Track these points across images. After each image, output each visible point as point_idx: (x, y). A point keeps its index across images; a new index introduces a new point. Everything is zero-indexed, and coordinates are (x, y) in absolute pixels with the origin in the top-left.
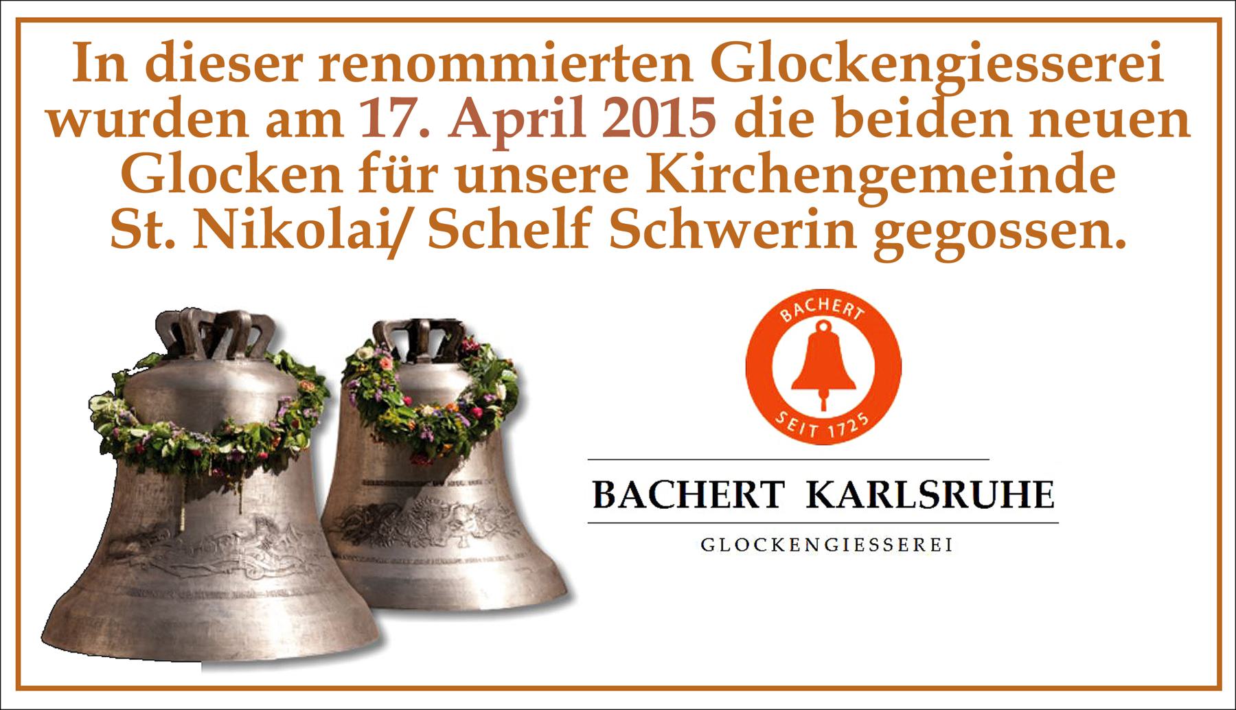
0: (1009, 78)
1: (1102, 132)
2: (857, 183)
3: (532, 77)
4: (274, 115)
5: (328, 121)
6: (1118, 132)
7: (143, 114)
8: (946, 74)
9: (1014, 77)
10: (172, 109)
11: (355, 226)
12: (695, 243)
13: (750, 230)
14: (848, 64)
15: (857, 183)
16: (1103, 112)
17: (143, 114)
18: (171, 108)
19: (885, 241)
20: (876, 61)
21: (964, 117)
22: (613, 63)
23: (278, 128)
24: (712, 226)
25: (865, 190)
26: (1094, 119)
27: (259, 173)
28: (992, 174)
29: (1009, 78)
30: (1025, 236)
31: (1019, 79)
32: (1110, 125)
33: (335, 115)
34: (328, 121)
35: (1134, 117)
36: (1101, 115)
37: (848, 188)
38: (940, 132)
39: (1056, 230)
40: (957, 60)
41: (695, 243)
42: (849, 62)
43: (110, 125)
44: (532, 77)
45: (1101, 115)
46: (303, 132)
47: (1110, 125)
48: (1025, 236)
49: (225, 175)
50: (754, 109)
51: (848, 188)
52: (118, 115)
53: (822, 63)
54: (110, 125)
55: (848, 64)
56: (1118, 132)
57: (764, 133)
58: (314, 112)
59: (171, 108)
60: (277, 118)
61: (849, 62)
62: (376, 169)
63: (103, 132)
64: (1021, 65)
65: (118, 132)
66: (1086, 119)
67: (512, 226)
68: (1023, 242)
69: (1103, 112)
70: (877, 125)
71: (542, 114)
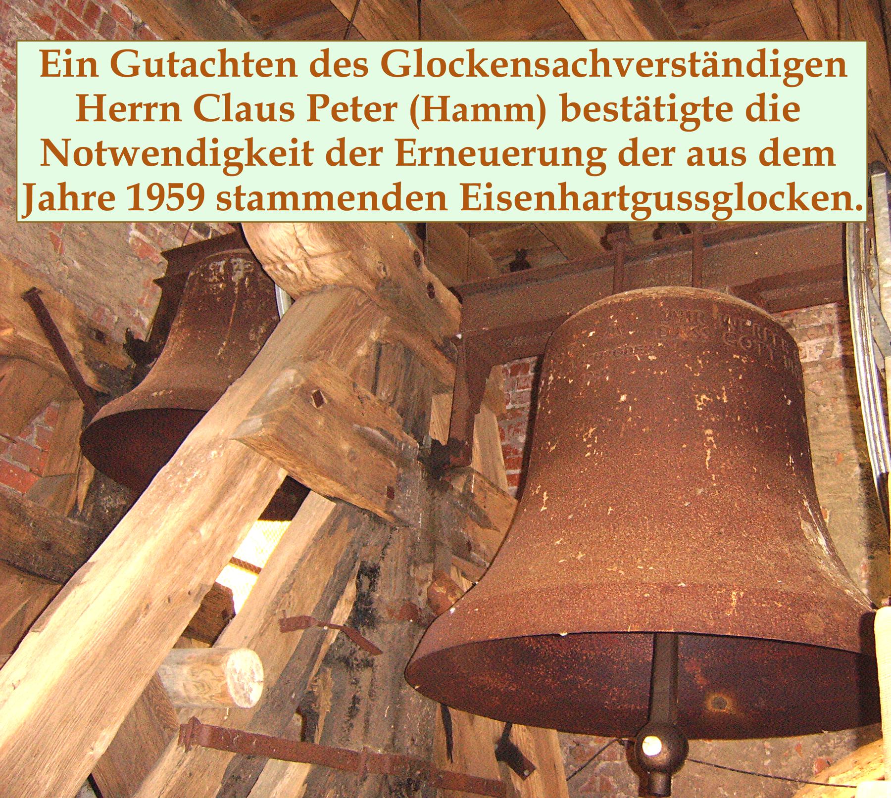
0: (598, 119)
1: (484, 163)
2: (585, 159)
3: (498, 119)
4: (692, 151)
5: (825, 155)
6: (495, 162)
7: (379, 150)
8: (687, 117)
9: (602, 118)
10: (339, 146)
11: (44, 196)
12: (607, 74)
13: (634, 65)
14: (475, 65)
15: (585, 159)
16: (544, 149)
17: (379, 150)
18: (631, 146)
19: (720, 206)
20: (815, 197)
21: (358, 152)
22: (618, 198)
23: (695, 160)
24: (618, 61)
25: (591, 164)
26: (478, 154)
27: (796, 197)
28: (284, 153)
29: (598, 119)
30: (694, 202)
31: (605, 119)
32: (489, 157)
33: (830, 151)
34: (825, 155)
35: (506, 152)
36: (483, 151)
37: (579, 163)
38: (775, 162)
39: (517, 198)
40: (646, 196)
41: (607, 74)
42: (254, 152)
43: (548, 157)
44: (498, 119)
45: (483, 151)
46: (727, 74)
47: (489, 157)
48: (694, 202)
49: (773, 197)
50: (199, 146)
51: (579, 163)
52: (554, 151)
53: (778, 198)
54: (548, 157)
55: (475, 65)
56: (495, 162)
57: (558, 163)
58: (815, 149)
59: (631, 146)
60: (695, 153)
61: (254, 152)
62: (106, 150)
63: (543, 163)
64: (606, 110)
65: (554, 162)
66: (473, 153)
67: (74, 195)
68: (693, 206)
69: (544, 149)
70: (509, 158)
71: (532, 150)
